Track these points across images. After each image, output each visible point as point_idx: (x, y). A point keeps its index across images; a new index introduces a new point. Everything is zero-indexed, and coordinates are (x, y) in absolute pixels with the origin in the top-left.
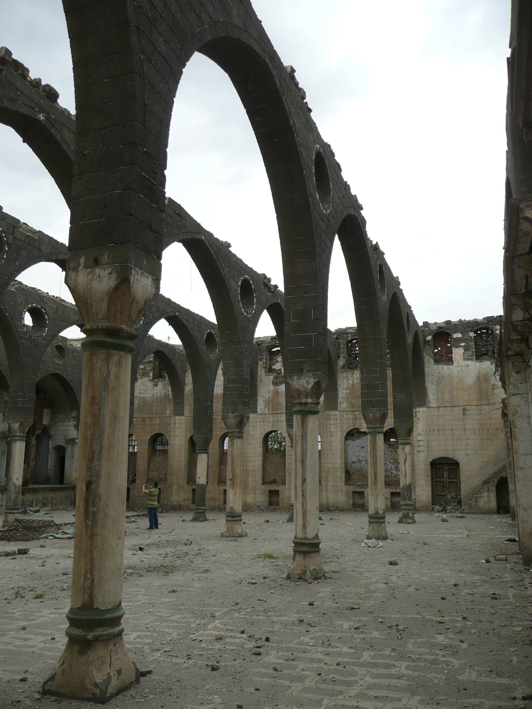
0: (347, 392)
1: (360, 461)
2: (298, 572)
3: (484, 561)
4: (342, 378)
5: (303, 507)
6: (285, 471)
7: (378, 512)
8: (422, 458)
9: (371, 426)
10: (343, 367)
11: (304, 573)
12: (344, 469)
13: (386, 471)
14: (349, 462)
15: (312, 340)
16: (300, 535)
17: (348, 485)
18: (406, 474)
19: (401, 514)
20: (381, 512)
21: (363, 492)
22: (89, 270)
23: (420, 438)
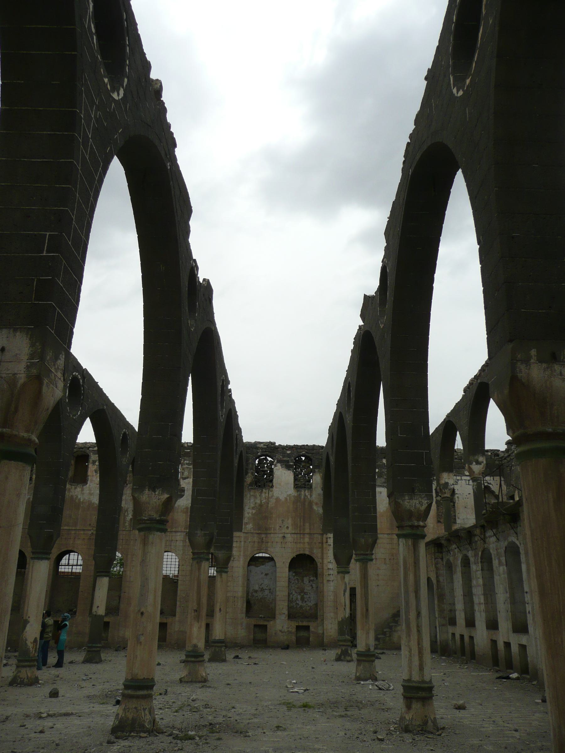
0: (254, 511)
1: (262, 590)
2: (418, 723)
3: (540, 701)
4: (248, 496)
5: (419, 644)
6: (176, 600)
7: (369, 649)
8: (332, 588)
9: (362, 552)
10: (251, 484)
11: (425, 723)
12: (245, 599)
13: (290, 601)
14: (251, 590)
15: (423, 458)
16: (416, 677)
17: (249, 617)
18: (345, 606)
19: (339, 651)
20: (372, 649)
21: (266, 626)
22: (544, 365)
23: (330, 566)
